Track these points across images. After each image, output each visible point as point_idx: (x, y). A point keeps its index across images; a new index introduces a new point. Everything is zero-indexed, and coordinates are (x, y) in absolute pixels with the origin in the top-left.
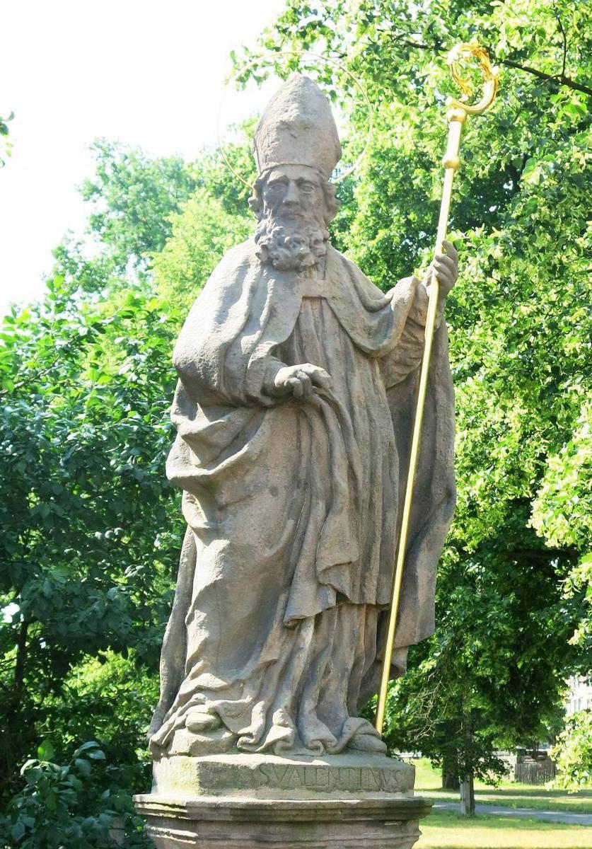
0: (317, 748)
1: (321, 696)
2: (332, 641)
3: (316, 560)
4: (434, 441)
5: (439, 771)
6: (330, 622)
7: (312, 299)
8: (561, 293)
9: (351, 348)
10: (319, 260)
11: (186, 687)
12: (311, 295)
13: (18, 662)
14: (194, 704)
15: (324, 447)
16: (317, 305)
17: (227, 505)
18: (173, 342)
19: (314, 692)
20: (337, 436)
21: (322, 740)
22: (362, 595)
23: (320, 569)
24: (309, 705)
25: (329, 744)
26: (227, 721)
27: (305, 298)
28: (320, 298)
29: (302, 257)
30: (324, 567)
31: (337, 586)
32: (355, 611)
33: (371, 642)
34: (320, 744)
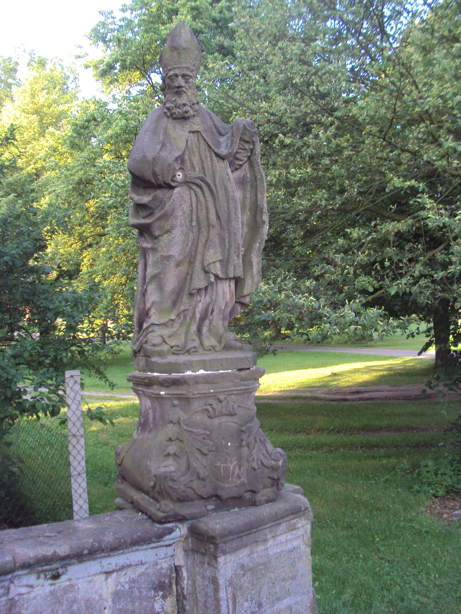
0: (210, 350)
1: (210, 323)
2: (214, 297)
3: (203, 260)
4: (256, 196)
5: (419, 393)
6: (212, 289)
7: (194, 132)
8: (15, 458)
9: (214, 155)
10: (195, 113)
11: (145, 326)
12: (193, 130)
13: (449, 327)
14: (151, 332)
15: (204, 205)
16: (196, 135)
17: (159, 236)
18: (121, 7)
19: (207, 322)
20: (209, 198)
21: (212, 346)
22: (227, 273)
23: (205, 265)
24: (205, 329)
25: (215, 348)
26: (167, 340)
27: (190, 132)
28: (197, 132)
29: (186, 112)
30: (207, 263)
31: (214, 272)
32: (224, 282)
33: (233, 296)
34: (211, 348)
